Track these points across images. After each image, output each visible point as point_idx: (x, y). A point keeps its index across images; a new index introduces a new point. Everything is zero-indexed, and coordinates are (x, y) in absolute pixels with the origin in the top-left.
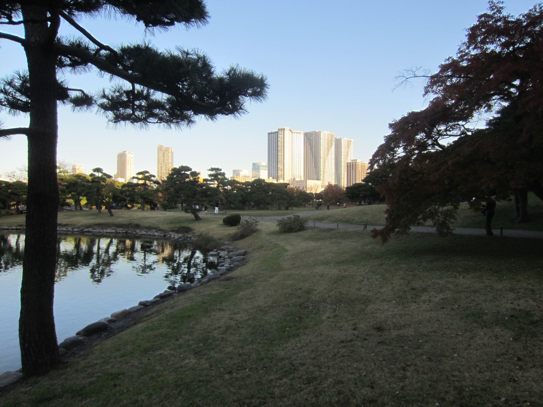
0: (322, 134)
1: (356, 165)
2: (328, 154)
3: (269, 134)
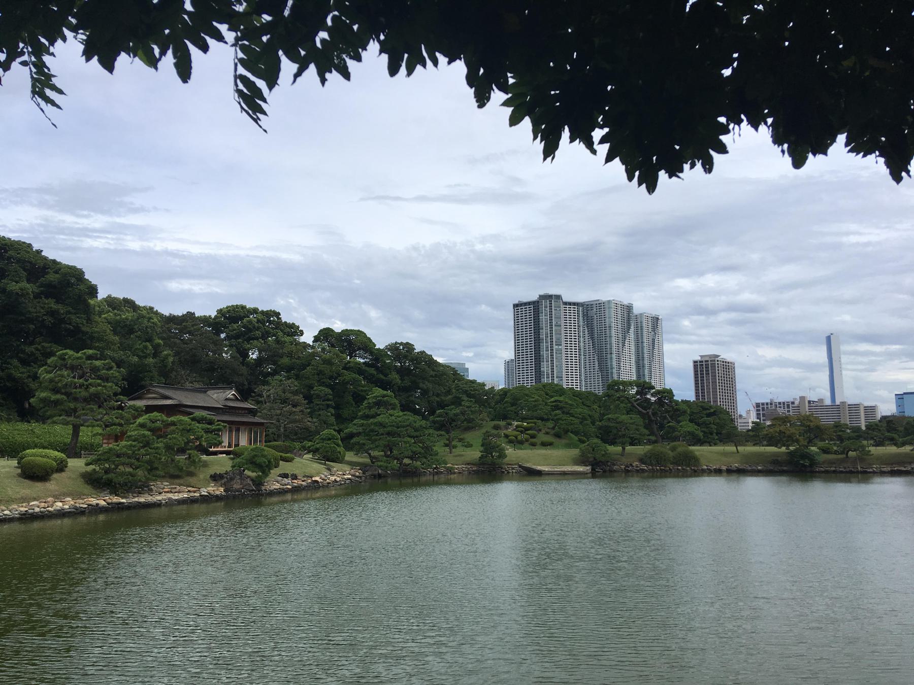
1: (713, 366)
2: (624, 345)
3: (515, 306)
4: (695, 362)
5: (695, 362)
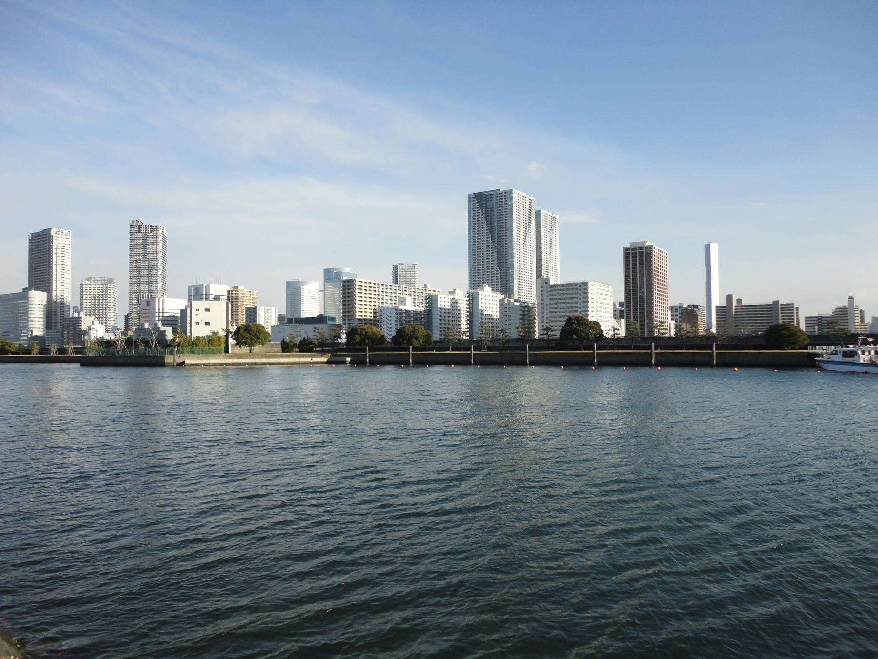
0: (514, 195)
4: (626, 250)
5: (626, 250)
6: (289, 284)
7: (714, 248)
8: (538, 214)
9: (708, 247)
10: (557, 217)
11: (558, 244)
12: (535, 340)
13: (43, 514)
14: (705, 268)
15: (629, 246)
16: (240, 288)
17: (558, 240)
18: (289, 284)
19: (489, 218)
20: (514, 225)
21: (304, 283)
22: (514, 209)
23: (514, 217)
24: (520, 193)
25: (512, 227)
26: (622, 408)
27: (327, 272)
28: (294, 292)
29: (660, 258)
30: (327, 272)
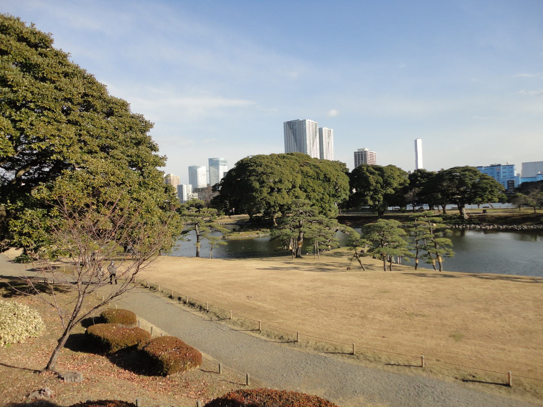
0: (307, 122)
4: (355, 153)
5: (355, 153)
6: (190, 168)
7: (419, 142)
8: (321, 130)
9: (416, 141)
10: (332, 130)
11: (333, 144)
12: (440, 199)
13: (79, 304)
14: (414, 153)
15: (357, 151)
16: (172, 175)
17: (332, 142)
18: (190, 168)
19: (294, 134)
20: (307, 138)
21: (198, 167)
22: (307, 129)
23: (307, 133)
24: (311, 121)
25: (306, 139)
26: (377, 244)
27: (210, 160)
28: (193, 173)
29: (372, 155)
30: (210, 160)
